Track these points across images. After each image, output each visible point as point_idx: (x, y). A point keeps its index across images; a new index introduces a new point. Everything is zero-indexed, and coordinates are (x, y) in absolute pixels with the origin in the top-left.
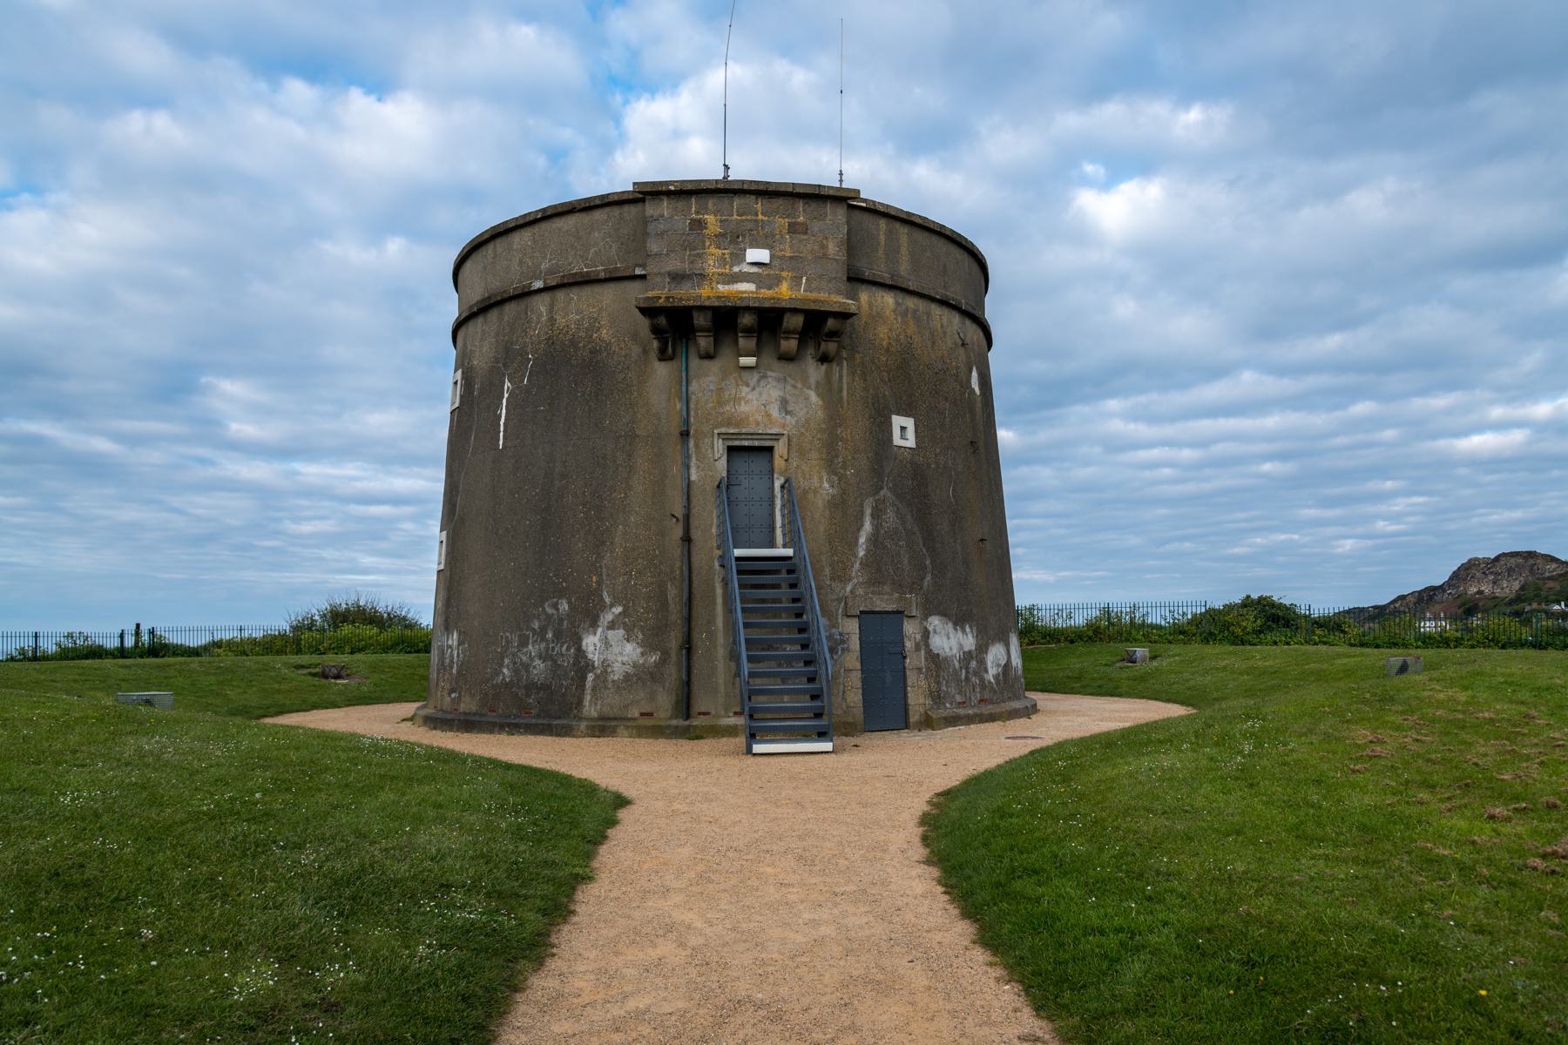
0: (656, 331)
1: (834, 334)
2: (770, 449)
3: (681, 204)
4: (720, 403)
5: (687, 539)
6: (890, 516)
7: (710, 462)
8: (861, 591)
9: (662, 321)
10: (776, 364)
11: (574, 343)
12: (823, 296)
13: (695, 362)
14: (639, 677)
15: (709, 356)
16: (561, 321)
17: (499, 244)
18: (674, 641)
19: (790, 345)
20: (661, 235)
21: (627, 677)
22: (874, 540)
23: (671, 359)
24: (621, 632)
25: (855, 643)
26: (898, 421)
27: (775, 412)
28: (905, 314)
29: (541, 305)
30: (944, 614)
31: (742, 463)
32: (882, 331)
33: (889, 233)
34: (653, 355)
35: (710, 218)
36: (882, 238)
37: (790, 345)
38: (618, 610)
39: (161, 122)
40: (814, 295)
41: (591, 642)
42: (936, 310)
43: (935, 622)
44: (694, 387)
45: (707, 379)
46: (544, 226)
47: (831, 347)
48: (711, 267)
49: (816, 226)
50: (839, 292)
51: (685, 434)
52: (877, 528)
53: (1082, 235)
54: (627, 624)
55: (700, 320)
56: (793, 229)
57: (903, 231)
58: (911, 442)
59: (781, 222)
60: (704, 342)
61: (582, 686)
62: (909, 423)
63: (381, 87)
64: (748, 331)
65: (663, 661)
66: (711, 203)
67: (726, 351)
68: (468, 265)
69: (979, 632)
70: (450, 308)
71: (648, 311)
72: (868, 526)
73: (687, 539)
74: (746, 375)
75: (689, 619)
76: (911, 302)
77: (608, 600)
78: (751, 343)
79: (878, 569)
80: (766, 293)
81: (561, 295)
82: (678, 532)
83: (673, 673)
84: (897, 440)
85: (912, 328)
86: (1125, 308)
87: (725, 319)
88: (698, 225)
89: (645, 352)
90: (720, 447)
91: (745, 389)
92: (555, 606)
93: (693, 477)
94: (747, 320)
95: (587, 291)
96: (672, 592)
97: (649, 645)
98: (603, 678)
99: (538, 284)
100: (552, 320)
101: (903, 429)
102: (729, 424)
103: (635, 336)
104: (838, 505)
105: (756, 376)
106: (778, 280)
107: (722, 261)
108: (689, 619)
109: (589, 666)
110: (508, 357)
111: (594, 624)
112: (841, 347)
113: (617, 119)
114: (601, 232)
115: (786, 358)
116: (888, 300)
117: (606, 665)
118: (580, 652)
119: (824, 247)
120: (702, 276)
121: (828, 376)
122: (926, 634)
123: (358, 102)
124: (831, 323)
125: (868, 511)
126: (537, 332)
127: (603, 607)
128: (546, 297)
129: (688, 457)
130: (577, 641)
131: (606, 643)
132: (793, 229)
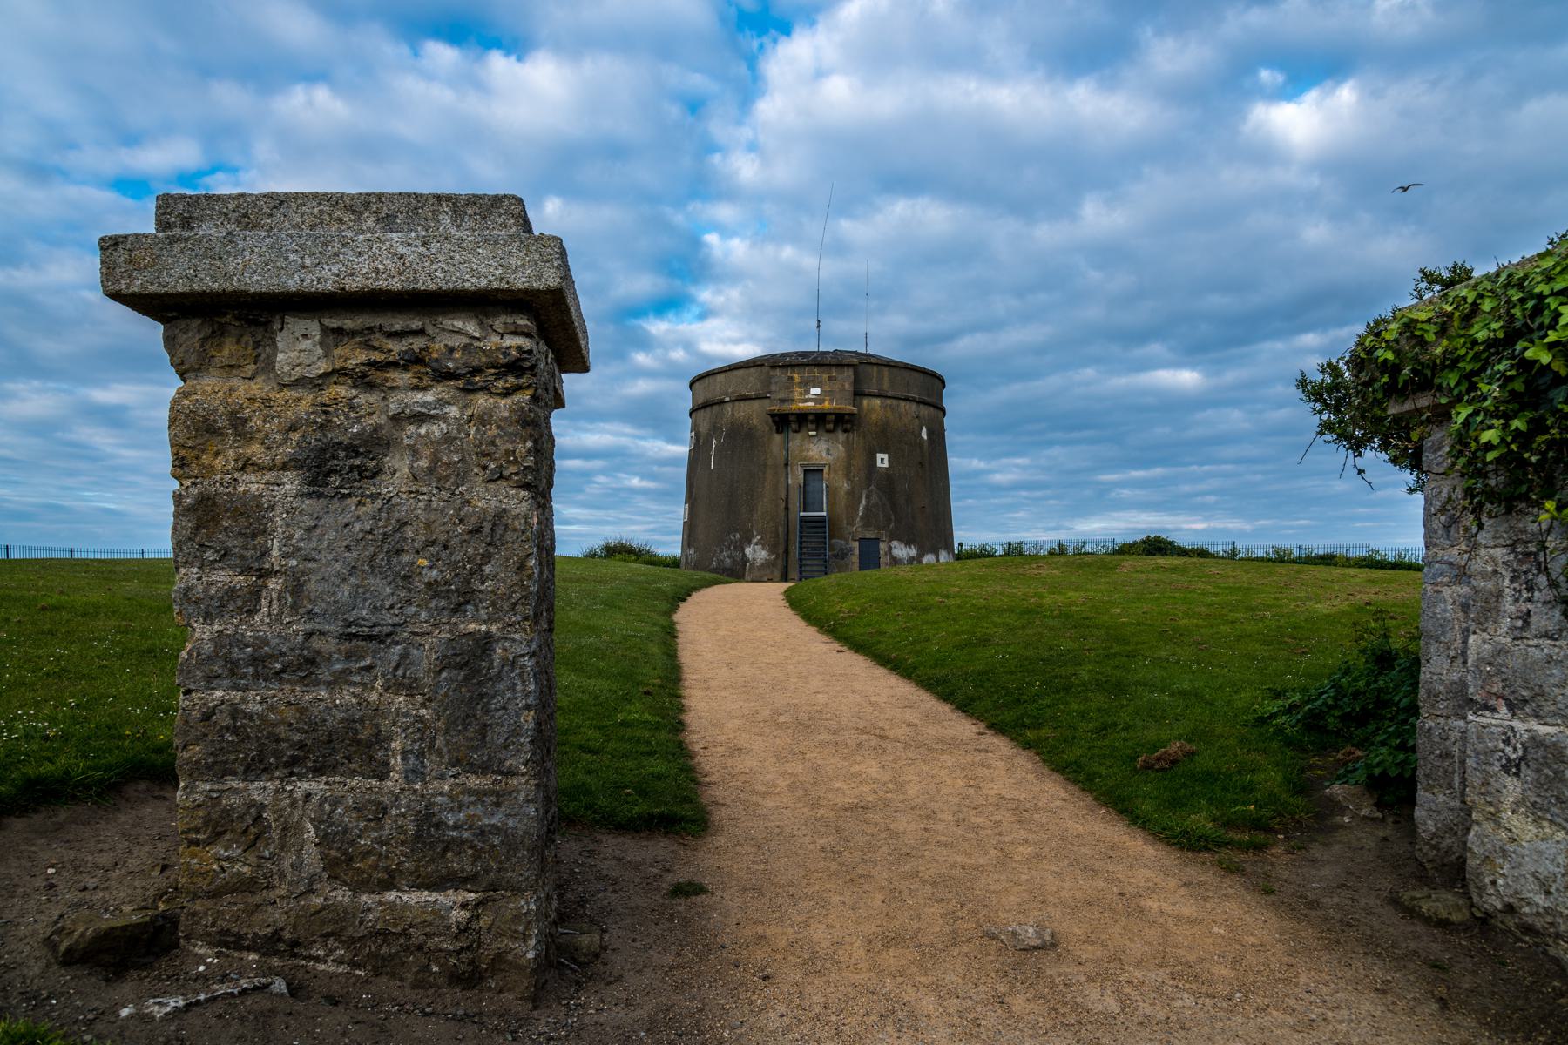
0: (774, 422)
1: (848, 421)
2: (822, 470)
3: (784, 370)
4: (801, 451)
5: (787, 508)
6: (875, 498)
7: (797, 477)
8: (859, 530)
9: (777, 419)
10: (825, 434)
11: (742, 425)
12: (843, 406)
13: (791, 434)
14: (767, 564)
15: (796, 432)
16: (737, 415)
17: (711, 379)
18: (781, 551)
19: (830, 426)
20: (776, 383)
21: (762, 565)
22: (867, 508)
23: (782, 432)
24: (760, 547)
25: (857, 551)
26: (879, 456)
27: (824, 454)
28: (885, 408)
29: (729, 408)
30: (900, 540)
31: (810, 477)
32: (874, 416)
33: (878, 372)
34: (774, 431)
35: (796, 376)
36: (875, 375)
37: (830, 426)
38: (759, 537)
39: (322, 94)
40: (838, 406)
41: (748, 551)
42: (903, 403)
43: (895, 543)
44: (790, 444)
45: (796, 441)
46: (729, 373)
47: (849, 426)
48: (797, 396)
49: (840, 377)
50: (849, 404)
51: (787, 465)
52: (868, 503)
53: (1266, 154)
54: (762, 543)
55: (791, 418)
56: (830, 379)
57: (886, 371)
58: (886, 464)
59: (825, 376)
60: (794, 426)
61: (745, 569)
62: (885, 456)
63: (518, 46)
64: (812, 422)
65: (777, 558)
66: (796, 370)
67: (804, 429)
68: (697, 384)
69: (919, 548)
70: (689, 406)
71: (772, 415)
72: (864, 502)
73: (787, 508)
74: (812, 439)
75: (787, 541)
76: (889, 402)
77: (755, 533)
78: (814, 426)
79: (868, 520)
80: (819, 406)
81: (737, 403)
82: (783, 505)
83: (780, 563)
84: (879, 464)
85: (889, 413)
86: (1316, 233)
87: (803, 419)
88: (791, 379)
89: (771, 429)
90: (800, 470)
91: (811, 445)
92: (734, 536)
93: (790, 482)
94: (811, 418)
95: (747, 403)
96: (781, 529)
97: (771, 552)
98: (752, 565)
99: (727, 399)
100: (733, 414)
101: (882, 459)
102: (805, 460)
103: (767, 423)
104: (850, 493)
105: (816, 439)
106: (824, 401)
107: (801, 393)
108: (787, 541)
109: (748, 560)
110: (715, 429)
111: (750, 543)
112: (853, 425)
113: (752, 61)
114: (753, 379)
115: (828, 431)
116: (878, 401)
117: (754, 559)
118: (744, 555)
119: (843, 385)
120: (793, 400)
121: (848, 438)
122: (890, 549)
123: (499, 63)
124: (846, 417)
125: (864, 496)
126: (727, 419)
127: (753, 536)
128: (731, 404)
129: (787, 474)
130: (743, 550)
131: (754, 551)
132: (830, 379)
